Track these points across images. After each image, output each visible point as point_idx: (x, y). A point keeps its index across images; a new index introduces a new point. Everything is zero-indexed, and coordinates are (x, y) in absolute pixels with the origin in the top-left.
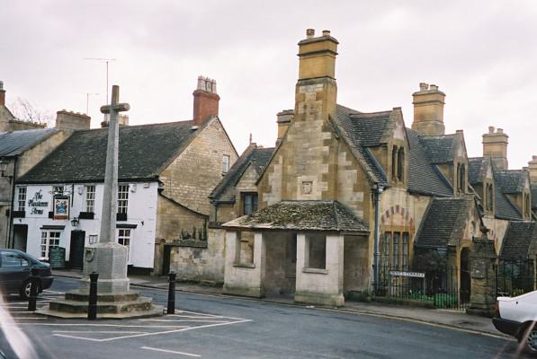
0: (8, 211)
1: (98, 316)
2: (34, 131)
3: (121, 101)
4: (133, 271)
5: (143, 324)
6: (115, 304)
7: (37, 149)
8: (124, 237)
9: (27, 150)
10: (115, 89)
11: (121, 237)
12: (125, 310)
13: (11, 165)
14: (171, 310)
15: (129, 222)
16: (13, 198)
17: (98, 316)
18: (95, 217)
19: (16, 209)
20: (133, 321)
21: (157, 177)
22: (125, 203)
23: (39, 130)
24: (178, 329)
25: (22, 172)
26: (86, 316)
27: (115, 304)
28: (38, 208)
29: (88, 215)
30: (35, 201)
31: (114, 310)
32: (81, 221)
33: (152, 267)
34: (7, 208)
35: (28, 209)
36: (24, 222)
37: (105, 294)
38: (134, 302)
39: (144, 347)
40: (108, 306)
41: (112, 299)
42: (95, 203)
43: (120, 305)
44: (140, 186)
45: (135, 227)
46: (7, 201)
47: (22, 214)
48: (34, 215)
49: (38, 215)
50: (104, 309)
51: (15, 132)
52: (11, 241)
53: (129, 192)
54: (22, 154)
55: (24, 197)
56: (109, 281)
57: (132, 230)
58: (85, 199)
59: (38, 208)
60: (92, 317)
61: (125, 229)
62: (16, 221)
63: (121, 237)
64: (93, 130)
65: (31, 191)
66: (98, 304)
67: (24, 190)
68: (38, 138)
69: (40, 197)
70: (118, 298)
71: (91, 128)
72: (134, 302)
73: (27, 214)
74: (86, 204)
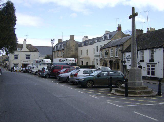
0: (121, 61)
1: (129, 95)
2: (128, 36)
3: (135, 12)
4: (144, 78)
5: (146, 99)
6: (135, 91)
7: (128, 42)
8: (153, 67)
9: (125, 42)
10: (133, 8)
11: (152, 67)
12: (140, 93)
13: (121, 47)
14: (160, 94)
15: (155, 62)
16: (122, 57)
17: (129, 95)
18: (144, 61)
19: (123, 60)
20: (142, 98)
21: (163, 46)
22: (153, 56)
23: (129, 36)
24: (157, 103)
25: (124, 49)
26: (124, 95)
27: (135, 91)
28: (129, 59)
29: (142, 61)
30: (128, 57)
31: (135, 93)
32: (140, 63)
33: (163, 78)
34: (121, 60)
35: (126, 60)
36: (126, 64)
37: (133, 87)
38: (144, 91)
39: (135, 112)
40: (133, 92)
41: (135, 89)
42: (144, 57)
43: (138, 91)
44: (157, 50)
45: (156, 64)
46: (121, 58)
47: (125, 62)
48: (128, 62)
49: (129, 62)
50: (131, 93)
51: (123, 38)
52: (123, 70)
53: (154, 52)
54: (124, 43)
55: (125, 56)
56: (134, 82)
57: (155, 65)
58: (141, 56)
59: (129, 59)
60: (126, 96)
61: (153, 65)
62: (124, 64)
63: (152, 67)
64: (144, 34)
65: (127, 54)
66: (129, 90)
67: (125, 54)
68: (129, 38)
69: (129, 56)
70: (138, 89)
71: (144, 33)
72: (144, 91)
73: (126, 62)
74: (141, 57)
